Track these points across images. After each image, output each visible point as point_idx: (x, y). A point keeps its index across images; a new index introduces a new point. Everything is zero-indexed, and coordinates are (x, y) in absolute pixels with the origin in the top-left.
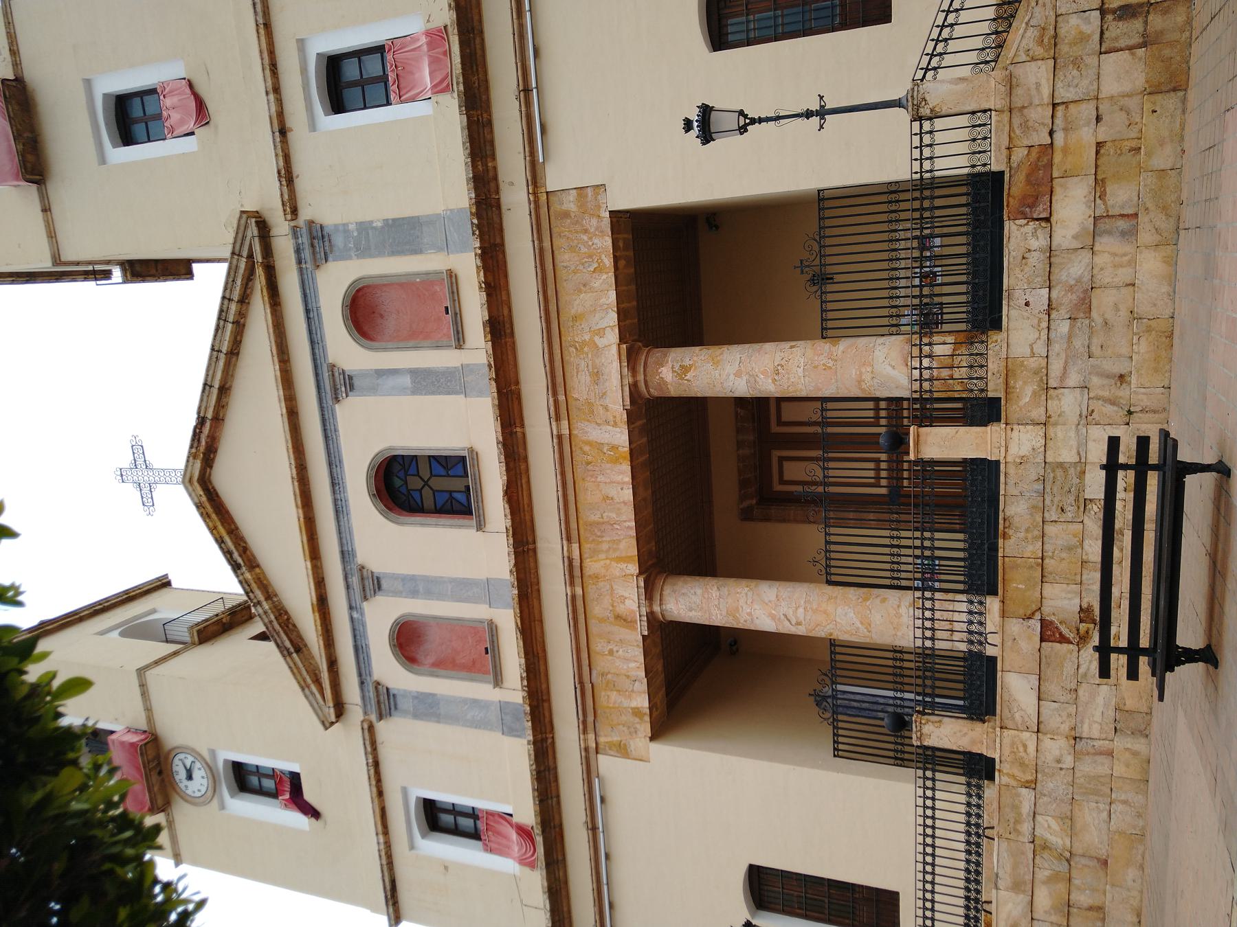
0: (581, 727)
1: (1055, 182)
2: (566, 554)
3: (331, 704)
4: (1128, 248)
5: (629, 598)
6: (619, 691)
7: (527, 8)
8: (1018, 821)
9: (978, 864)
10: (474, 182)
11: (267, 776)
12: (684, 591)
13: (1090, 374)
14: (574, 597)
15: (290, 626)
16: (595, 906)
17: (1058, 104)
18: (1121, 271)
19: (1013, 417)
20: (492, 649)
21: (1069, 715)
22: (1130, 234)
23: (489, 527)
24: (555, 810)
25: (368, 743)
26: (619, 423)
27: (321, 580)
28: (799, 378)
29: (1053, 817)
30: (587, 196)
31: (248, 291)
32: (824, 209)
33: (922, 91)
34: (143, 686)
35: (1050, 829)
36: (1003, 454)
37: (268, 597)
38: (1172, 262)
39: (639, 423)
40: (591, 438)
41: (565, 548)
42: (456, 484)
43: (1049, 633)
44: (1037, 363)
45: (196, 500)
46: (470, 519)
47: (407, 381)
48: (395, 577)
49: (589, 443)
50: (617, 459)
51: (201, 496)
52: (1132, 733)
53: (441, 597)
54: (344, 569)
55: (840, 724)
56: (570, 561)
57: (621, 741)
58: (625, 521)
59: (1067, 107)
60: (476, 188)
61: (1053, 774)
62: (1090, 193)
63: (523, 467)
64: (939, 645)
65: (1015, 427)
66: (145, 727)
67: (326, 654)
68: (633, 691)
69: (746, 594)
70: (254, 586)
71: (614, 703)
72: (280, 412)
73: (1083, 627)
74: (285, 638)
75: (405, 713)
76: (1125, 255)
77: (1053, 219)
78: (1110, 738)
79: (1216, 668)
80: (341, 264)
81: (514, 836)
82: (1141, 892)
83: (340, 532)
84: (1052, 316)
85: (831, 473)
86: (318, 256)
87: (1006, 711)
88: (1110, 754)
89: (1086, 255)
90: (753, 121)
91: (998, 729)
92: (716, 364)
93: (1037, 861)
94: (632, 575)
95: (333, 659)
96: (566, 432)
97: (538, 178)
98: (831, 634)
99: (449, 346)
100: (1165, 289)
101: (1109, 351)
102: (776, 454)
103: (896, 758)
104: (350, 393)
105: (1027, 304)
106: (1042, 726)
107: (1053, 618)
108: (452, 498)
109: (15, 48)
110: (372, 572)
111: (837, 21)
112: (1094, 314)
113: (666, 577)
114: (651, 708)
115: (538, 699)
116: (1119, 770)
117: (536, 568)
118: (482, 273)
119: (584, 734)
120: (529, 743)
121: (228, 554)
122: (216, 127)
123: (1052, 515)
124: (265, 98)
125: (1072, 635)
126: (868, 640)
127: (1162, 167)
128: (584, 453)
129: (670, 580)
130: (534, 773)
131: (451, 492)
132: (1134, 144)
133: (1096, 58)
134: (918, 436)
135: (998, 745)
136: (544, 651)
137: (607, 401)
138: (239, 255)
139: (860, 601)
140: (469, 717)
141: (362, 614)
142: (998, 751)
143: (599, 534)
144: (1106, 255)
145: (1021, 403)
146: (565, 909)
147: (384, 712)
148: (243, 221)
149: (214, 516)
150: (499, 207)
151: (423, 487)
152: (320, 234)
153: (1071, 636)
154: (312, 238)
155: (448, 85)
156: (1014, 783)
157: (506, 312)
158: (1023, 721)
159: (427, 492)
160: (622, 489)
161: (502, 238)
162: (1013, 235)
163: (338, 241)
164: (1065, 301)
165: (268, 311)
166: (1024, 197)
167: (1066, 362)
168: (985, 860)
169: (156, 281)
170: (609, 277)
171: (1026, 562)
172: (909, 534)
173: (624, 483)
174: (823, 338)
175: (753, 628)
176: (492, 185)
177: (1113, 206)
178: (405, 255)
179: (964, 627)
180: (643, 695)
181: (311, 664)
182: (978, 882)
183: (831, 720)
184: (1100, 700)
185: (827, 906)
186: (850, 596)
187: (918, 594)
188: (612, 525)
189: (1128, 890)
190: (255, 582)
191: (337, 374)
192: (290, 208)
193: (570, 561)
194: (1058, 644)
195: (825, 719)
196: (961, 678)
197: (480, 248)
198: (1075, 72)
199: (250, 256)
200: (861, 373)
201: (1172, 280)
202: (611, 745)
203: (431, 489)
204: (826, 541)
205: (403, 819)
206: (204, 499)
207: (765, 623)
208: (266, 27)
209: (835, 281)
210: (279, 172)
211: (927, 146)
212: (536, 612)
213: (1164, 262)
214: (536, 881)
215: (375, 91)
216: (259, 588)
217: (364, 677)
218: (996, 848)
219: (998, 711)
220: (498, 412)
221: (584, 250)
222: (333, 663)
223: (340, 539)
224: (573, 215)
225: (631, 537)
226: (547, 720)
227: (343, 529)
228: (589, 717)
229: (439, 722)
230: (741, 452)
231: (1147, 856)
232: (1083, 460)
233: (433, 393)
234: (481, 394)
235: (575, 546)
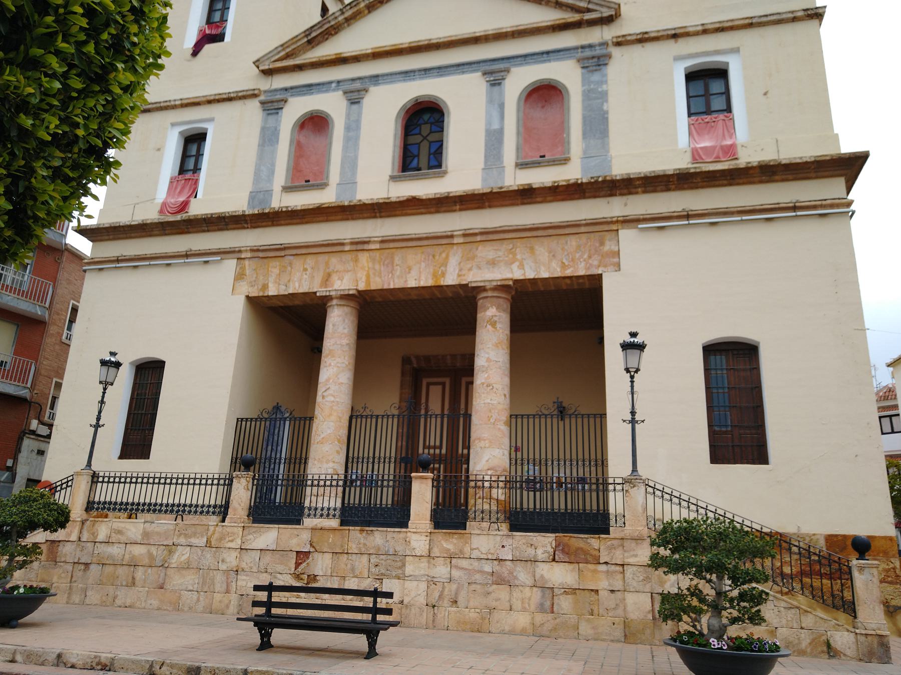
0: (255, 248)
1: (576, 565)
3: (271, 67)
4: (533, 608)
6: (279, 275)
7: (744, 218)
8: (186, 536)
9: (160, 511)
10: (627, 179)
11: (222, 15)
12: (346, 321)
13: (459, 583)
14: (342, 244)
15: (326, 36)
16: (135, 256)
17: (623, 567)
18: (519, 603)
19: (434, 537)
20: (308, 185)
21: (251, 568)
22: (541, 608)
23: (392, 184)
24: (199, 229)
25: (245, 93)
26: (459, 278)
28: (484, 400)
29: (189, 557)
31: (564, 8)
32: (595, 418)
33: (639, 485)
35: (181, 555)
36: (412, 530)
38: (523, 632)
39: (461, 292)
41: (376, 239)
42: (424, 160)
43: (302, 556)
44: (467, 552)
46: (399, 169)
47: (496, 126)
48: (360, 114)
49: (447, 257)
52: (240, 605)
53: (345, 148)
54: (365, 77)
55: (258, 423)
57: (246, 275)
58: (394, 281)
59: (621, 573)
60: (623, 180)
61: (215, 558)
62: (568, 586)
63: (432, 210)
64: (308, 489)
65: (428, 538)
67: (307, 63)
68: (279, 284)
69: (343, 363)
70: (355, 9)
71: (272, 272)
72: (477, 31)
73: (305, 577)
75: (265, 121)
77: (554, 563)
78: (238, 592)
79: (257, 650)
81: (182, 199)
82: (144, 608)
83: (391, 74)
84: (495, 562)
85: (433, 420)
86: (586, 61)
87: (254, 530)
88: (228, 591)
89: (530, 582)
90: (632, 377)
91: (243, 525)
92: (496, 345)
93: (162, 547)
94: (357, 286)
95: (303, 68)
96: (456, 241)
97: (627, 224)
98: (316, 418)
99: (518, 157)
100: (507, 628)
101: (472, 595)
102: (447, 381)
103: (236, 459)
104: (489, 84)
105: (503, 546)
106: (244, 551)
107: (311, 559)
108: (414, 157)
110: (363, 98)
111: (717, 429)
112: (495, 586)
113: (355, 308)
115: (273, 218)
116: (218, 597)
117: (364, 218)
118: (564, 183)
119: (251, 250)
120: (244, 211)
123: (374, 559)
124: (699, 23)
125: (300, 570)
126: (312, 442)
127: (580, 628)
128: (441, 254)
129: (354, 312)
130: (223, 215)
131: (418, 156)
132: (596, 612)
133: (648, 590)
134: (426, 478)
135: (233, 524)
136: (307, 223)
137: (475, 270)
139: (338, 437)
140: (262, 168)
141: (334, 90)
142: (229, 525)
143: (386, 263)
144: (530, 594)
146: (133, 235)
147: (266, 105)
148: (613, 5)
150: (611, 195)
151: (423, 136)
152: (601, 63)
153: (300, 569)
154: (599, 58)
155: (697, 160)
157: (538, 199)
158: (248, 540)
159: (418, 139)
160: (415, 280)
161: (589, 197)
162: (546, 539)
163: (596, 77)
164: (504, 570)
165: (549, 24)
167: (466, 569)
168: (163, 515)
170: (558, 273)
171: (345, 543)
172: (392, 472)
173: (420, 281)
174: (511, 416)
175: (322, 366)
176: (625, 191)
177: (559, 599)
178: (583, 127)
179: (320, 505)
180: (277, 291)
181: (300, 51)
182: (149, 510)
183: (261, 417)
185: (140, 412)
186: (341, 431)
187: (343, 478)
189: (145, 601)
190: (357, 10)
191: (502, 74)
192: (620, 41)
194: (295, 562)
195: (262, 413)
196: (288, 501)
198: (641, 578)
199: (589, 10)
200: (485, 440)
201: (512, 632)
203: (422, 141)
204: (378, 416)
205: (193, 118)
207: (325, 374)
208: (750, 24)
209: (560, 422)
210: (646, 33)
211: (615, 487)
212: (333, 218)
213: (523, 628)
214: (150, 214)
215: (699, 104)
216: (353, 13)
218: (170, 522)
219: (254, 525)
220: (470, 193)
221: (577, 255)
222: (300, 68)
223: (387, 75)
224: (601, 248)
225: (383, 285)
226: (260, 224)
227: (394, 76)
228: (263, 253)
229: (259, 146)
230: (448, 357)
231: (166, 612)
232: (406, 578)
233: (486, 145)
234: (484, 180)
235: (377, 246)
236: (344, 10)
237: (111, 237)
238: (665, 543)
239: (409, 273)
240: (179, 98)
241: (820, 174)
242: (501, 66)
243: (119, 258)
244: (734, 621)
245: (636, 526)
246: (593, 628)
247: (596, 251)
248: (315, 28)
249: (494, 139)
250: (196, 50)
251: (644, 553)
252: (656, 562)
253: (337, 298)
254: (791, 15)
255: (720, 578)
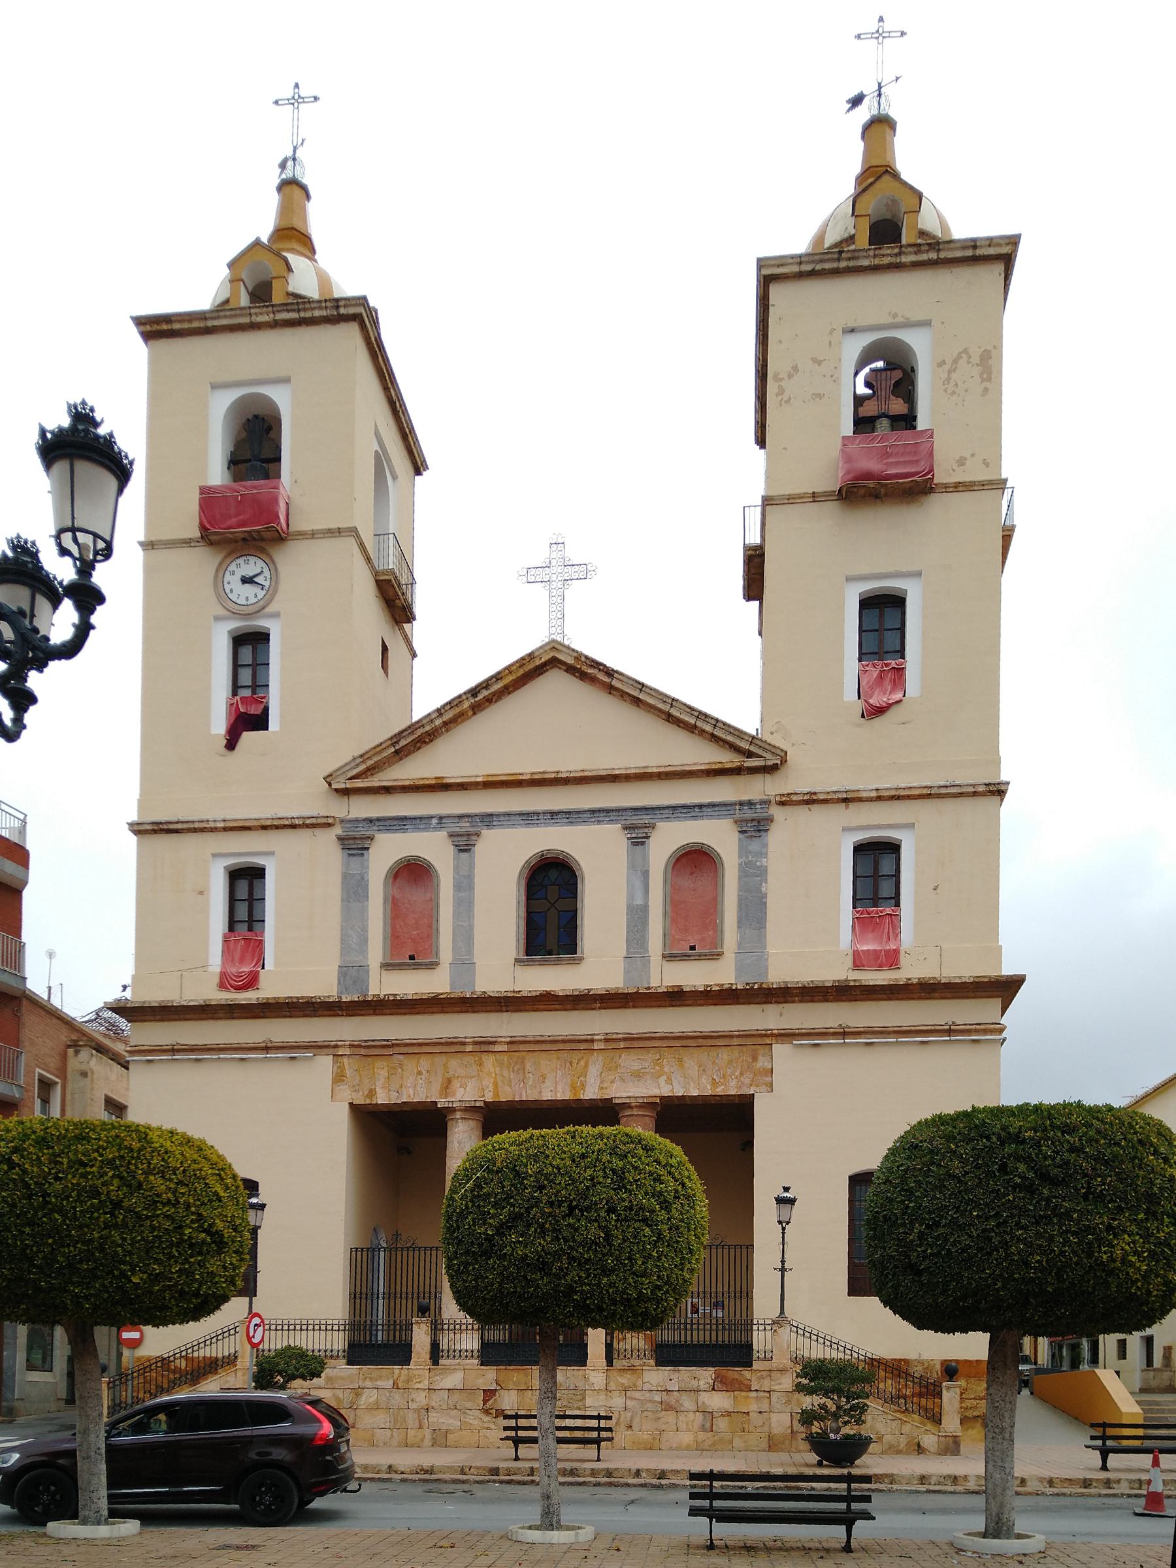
2: (499, 1040)
4: (696, 1428)
5: (465, 1092)
6: (389, 1078)
14: (464, 1044)
15: (418, 745)
19: (610, 1373)
22: (703, 1428)
27: (465, 787)
30: (767, 1077)
34: (338, 532)
37: (445, 724)
40: (590, 1067)
41: (503, 1039)
45: (537, 654)
48: (472, 866)
50: (574, 1088)
51: (541, 658)
53: (457, 915)
56: (493, 1043)
63: (568, 1007)
66: (291, 529)
68: (390, 1090)
70: (457, 710)
71: (379, 1074)
74: (409, 739)
76: (692, 1426)
80: (736, 848)
86: (744, 824)
88: (420, 1427)
90: (784, 1229)
94: (484, 1096)
100: (674, 1445)
105: (671, 1380)
109: (960, 489)
114: (377, 1104)
115: (376, 1006)
116: (411, 1433)
118: (718, 988)
121: (485, 684)
122: (859, 725)
129: (480, 1126)
131: (545, 929)
132: (746, 1430)
136: (418, 1013)
138: (751, 742)
141: (435, 829)
143: (516, 1068)
145: (618, 1377)
146: (188, 1016)
148: (779, 752)
149: (521, 672)
156: (395, 1377)
160: (551, 1091)
163: (754, 846)
164: (672, 1399)
165: (703, 767)
166: (726, 1377)
169: (744, 571)
173: (556, 1093)
176: (782, 999)
184: (451, 1421)
188: (523, 1080)
191: (646, 830)
193: (493, 1043)
197: (736, 988)
202: (341, 1068)
205: (246, 849)
206: (538, 662)
208: (929, 795)
210: (815, 793)
217: (377, 824)
221: (729, 1071)
228: (366, 1050)
229: (342, 900)
235: (505, 1048)
236: (443, 711)
237: (158, 1017)
238: (805, 1375)
239: (544, 1082)
240: (222, 817)
241: (978, 994)
242: (646, 819)
243: (175, 1047)
244: (845, 1423)
245: (781, 1359)
246: (745, 1442)
247: (748, 1067)
248: (405, 733)
249: (637, 917)
250: (231, 745)
251: (787, 1382)
252: (799, 1388)
253: (460, 1110)
254: (971, 789)
255: (839, 1398)
